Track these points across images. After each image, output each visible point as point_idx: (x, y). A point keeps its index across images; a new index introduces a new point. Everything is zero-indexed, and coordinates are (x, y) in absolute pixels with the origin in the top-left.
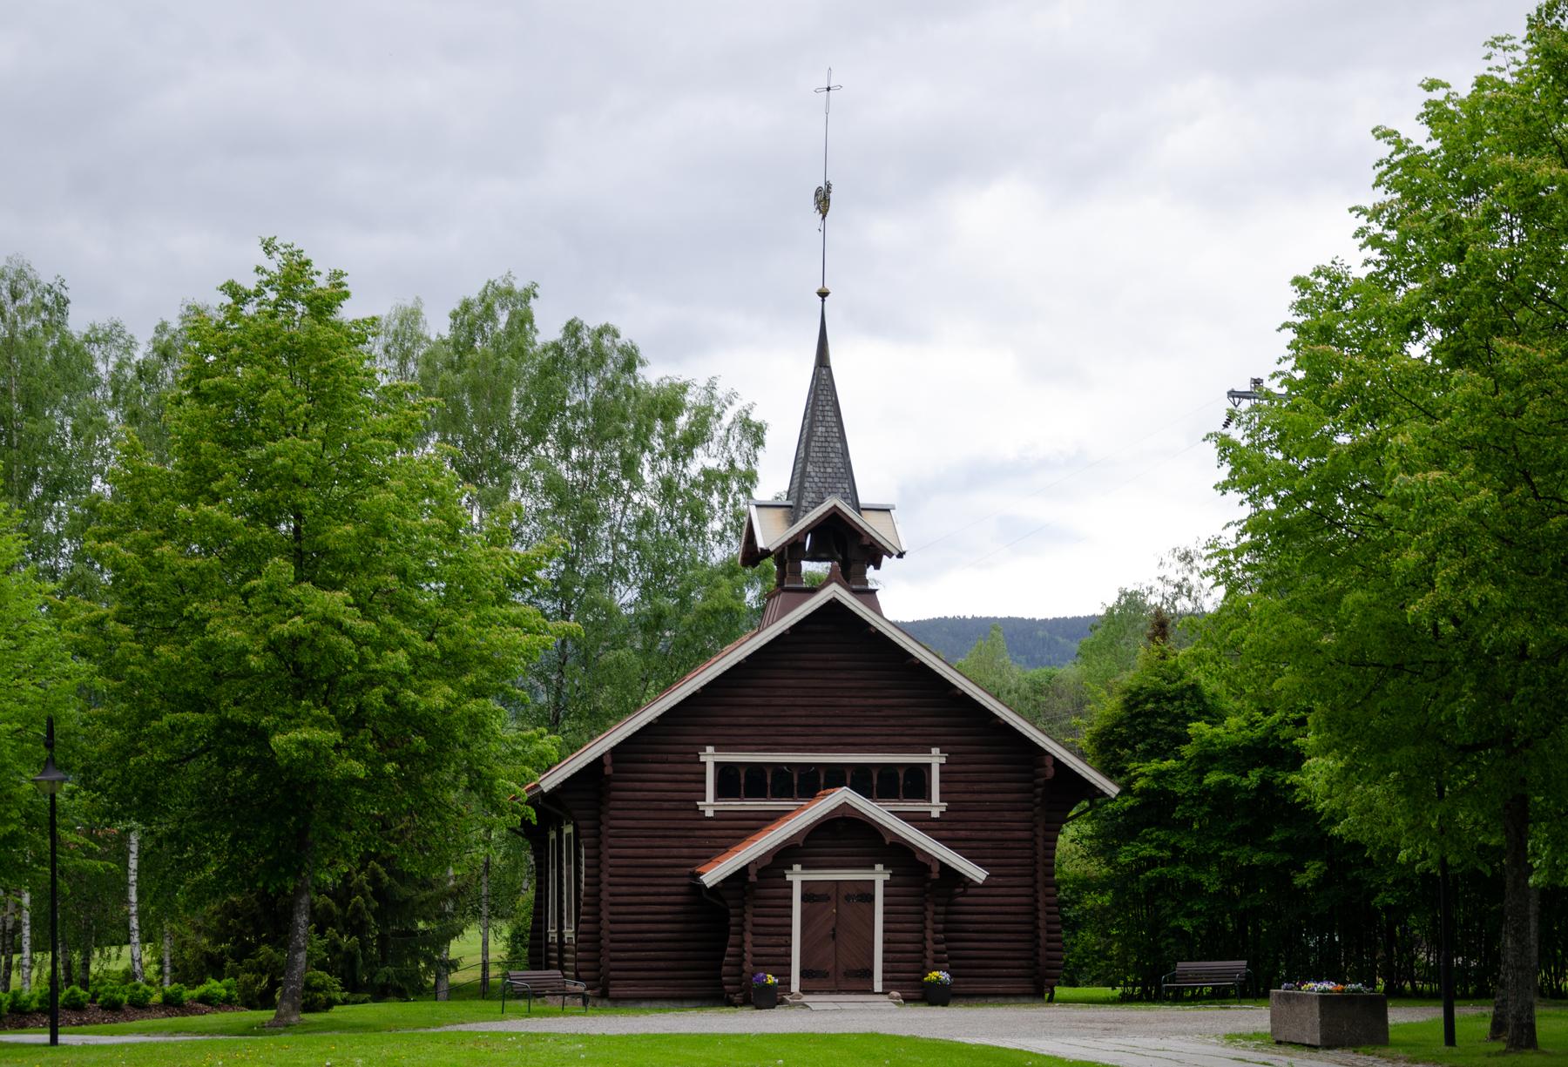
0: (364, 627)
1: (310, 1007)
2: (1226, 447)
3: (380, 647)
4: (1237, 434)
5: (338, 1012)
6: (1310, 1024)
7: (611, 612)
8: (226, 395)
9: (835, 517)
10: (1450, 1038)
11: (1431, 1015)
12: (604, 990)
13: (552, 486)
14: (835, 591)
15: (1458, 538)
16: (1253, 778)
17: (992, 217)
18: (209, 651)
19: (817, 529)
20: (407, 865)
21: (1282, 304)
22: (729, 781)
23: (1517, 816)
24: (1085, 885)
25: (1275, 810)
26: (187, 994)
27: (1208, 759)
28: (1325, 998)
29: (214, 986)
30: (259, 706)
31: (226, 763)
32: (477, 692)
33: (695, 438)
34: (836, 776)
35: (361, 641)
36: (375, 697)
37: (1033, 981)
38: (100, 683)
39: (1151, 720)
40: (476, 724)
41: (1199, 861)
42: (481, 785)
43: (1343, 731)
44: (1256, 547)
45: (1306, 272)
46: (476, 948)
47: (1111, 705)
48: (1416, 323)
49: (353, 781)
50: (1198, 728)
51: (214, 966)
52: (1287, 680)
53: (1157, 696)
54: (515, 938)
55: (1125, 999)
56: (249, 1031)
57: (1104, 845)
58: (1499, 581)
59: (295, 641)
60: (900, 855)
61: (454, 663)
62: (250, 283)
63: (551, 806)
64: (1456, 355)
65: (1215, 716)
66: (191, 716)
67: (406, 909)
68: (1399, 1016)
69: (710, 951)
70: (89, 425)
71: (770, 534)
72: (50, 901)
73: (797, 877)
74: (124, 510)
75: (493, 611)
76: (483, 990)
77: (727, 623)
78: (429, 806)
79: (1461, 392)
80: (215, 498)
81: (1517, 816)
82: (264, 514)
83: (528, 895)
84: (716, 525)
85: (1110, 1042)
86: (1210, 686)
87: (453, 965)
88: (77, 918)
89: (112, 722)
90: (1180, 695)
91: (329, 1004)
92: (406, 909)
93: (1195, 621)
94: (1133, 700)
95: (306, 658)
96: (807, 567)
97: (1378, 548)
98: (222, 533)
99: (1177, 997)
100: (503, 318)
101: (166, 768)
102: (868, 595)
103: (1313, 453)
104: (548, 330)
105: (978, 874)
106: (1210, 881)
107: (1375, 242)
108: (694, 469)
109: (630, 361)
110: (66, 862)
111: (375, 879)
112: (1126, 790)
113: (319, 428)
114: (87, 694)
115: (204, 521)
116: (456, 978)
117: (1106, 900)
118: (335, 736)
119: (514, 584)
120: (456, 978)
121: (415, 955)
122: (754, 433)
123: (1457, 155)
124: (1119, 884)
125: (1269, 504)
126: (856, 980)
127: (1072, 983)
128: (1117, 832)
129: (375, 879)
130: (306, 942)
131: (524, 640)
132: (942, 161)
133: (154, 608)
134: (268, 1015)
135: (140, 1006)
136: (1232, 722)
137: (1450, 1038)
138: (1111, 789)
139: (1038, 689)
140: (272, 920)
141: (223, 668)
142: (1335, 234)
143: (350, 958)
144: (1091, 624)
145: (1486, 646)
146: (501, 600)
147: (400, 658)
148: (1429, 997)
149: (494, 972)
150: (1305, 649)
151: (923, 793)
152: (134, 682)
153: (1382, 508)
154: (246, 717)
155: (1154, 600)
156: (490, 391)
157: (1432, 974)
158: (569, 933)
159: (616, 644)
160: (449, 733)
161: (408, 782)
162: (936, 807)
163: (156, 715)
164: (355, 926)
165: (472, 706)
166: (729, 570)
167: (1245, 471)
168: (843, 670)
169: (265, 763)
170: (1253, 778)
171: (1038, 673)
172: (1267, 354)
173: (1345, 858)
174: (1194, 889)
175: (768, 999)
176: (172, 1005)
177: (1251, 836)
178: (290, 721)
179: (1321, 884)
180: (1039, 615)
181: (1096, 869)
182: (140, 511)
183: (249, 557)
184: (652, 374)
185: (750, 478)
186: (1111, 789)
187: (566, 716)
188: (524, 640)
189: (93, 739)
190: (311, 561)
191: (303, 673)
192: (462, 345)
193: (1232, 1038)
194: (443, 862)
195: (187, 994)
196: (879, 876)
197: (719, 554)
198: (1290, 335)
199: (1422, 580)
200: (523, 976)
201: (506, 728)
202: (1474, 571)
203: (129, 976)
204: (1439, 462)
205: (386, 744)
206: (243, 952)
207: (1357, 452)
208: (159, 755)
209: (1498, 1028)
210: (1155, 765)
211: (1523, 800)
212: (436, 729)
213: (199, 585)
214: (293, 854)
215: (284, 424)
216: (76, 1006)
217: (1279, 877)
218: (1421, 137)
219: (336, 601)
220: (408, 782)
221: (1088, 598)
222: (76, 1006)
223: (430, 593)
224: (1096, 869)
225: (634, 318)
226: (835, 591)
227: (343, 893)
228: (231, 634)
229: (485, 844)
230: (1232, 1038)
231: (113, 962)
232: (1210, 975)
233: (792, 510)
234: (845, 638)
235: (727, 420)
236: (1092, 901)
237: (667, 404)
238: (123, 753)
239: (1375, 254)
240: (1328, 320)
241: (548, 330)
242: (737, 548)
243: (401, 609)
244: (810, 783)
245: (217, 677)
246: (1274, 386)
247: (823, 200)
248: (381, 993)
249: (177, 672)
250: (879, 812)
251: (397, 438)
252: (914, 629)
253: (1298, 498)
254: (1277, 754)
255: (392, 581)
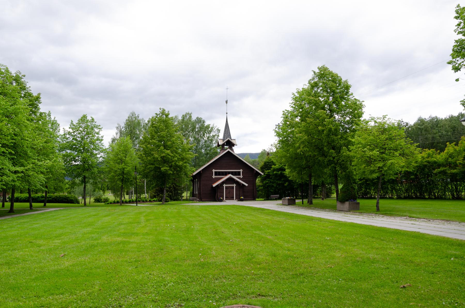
0: (172, 155)
1: (166, 202)
2: (275, 131)
3: (174, 157)
4: (277, 130)
5: (169, 202)
6: (286, 202)
7: (201, 153)
8: (155, 127)
9: (228, 141)
10: (303, 204)
11: (301, 201)
12: (201, 200)
13: (194, 137)
14: (229, 150)
15: (303, 142)
16: (279, 172)
17: (248, 102)
18: (154, 158)
19: (226, 142)
20: (177, 184)
21: (281, 114)
22: (216, 174)
23: (310, 176)
24: (259, 186)
25: (282, 176)
26: (152, 200)
27: (274, 170)
28: (288, 199)
29: (155, 199)
30: (159, 165)
31: (155, 171)
32: (185, 163)
33: (211, 131)
34: (229, 173)
35: (171, 156)
36: (173, 163)
37: (253, 198)
38: (141, 162)
39: (267, 166)
40: (185, 167)
41: (273, 183)
42: (186, 174)
43: (290, 166)
44: (279, 143)
45: (284, 110)
46: (186, 195)
47: (263, 163)
48: (297, 116)
49: (170, 174)
50: (273, 166)
51: (155, 197)
52: (283, 160)
53: (268, 162)
54: (190, 193)
55: (265, 200)
56: (159, 204)
57: (262, 180)
58: (308, 147)
59: (164, 157)
60: (237, 183)
61: (183, 159)
62: (158, 113)
63: (194, 177)
64: (302, 120)
65: (275, 165)
66: (152, 166)
67: (178, 190)
68: (297, 201)
69: (214, 195)
70: (140, 131)
71: (221, 143)
72: (136, 189)
73: (225, 185)
74: (144, 141)
75: (187, 153)
76: (187, 200)
77: (216, 154)
78: (180, 177)
79: (303, 125)
80: (154, 139)
81: (310, 176)
82: (160, 141)
83: (192, 188)
84: (214, 142)
85: (263, 205)
86: (274, 161)
87: (183, 197)
88: (139, 191)
89: (142, 167)
90: (271, 162)
91: (168, 201)
92: (178, 190)
93: (272, 153)
94: (265, 163)
95: (165, 159)
96: (225, 147)
97: (294, 144)
98: (155, 143)
99: (271, 200)
100: (188, 117)
101: (149, 172)
102: (232, 150)
103: (286, 133)
104: (194, 118)
105: (247, 185)
106: (275, 185)
107: (292, 107)
108: (211, 135)
109: (204, 122)
110: (138, 183)
111: (173, 186)
112: (264, 174)
113: (166, 130)
114: (140, 163)
115: (153, 142)
116: (183, 198)
117: (262, 188)
118: (168, 168)
119: (190, 149)
120: (183, 198)
121: (179, 196)
122: (219, 131)
123: (300, 97)
124: (263, 186)
125: (281, 138)
126: (232, 198)
127: (258, 198)
128: (263, 179)
129: (173, 186)
130: (166, 194)
131: (191, 156)
132: (243, 95)
133: (147, 153)
134: (161, 203)
135: (146, 201)
136: (277, 165)
137: (303, 204)
138: (263, 174)
139: (253, 162)
140: (161, 191)
141: (156, 160)
142: (287, 105)
143: (171, 196)
144: (259, 154)
145: (307, 156)
146: (188, 151)
147: (176, 159)
148: (300, 199)
149: (188, 198)
150: (285, 156)
151: (240, 175)
152: (145, 162)
153: (294, 139)
154: (158, 166)
155: (268, 150)
156: (187, 126)
157: (301, 196)
158: (197, 193)
159: (202, 157)
160: (182, 168)
161: (177, 174)
162: (241, 177)
163: (148, 166)
164: (172, 192)
165: (185, 164)
166: (216, 147)
167: (278, 135)
168: (231, 160)
169: (160, 172)
170: (279, 172)
171: (253, 160)
172: (279, 120)
173: (290, 182)
174: (273, 186)
175: (221, 201)
176: (150, 201)
177: (280, 180)
178: (163, 166)
179: (288, 185)
180: (254, 152)
181: (261, 184)
182: (146, 141)
183: (158, 146)
184: (206, 124)
185: (218, 136)
186: (263, 174)
187: (197, 165)
188: (191, 156)
189: (141, 169)
190: (166, 147)
191: (165, 160)
192: (183, 120)
193: (277, 204)
194: (182, 184)
195: (152, 200)
196: (235, 185)
197: (215, 145)
198: (283, 118)
199: (299, 148)
200: (191, 198)
201: (189, 167)
202: (305, 146)
203: (145, 198)
204: (301, 133)
205: (174, 169)
206: (158, 195)
207: (291, 132)
208: (148, 171)
209: (308, 202)
210: (268, 171)
211: (311, 174)
212: (181, 167)
213: (152, 150)
214: (164, 183)
215: (162, 130)
216: (139, 201)
217: (283, 184)
218: (297, 95)
219: (168, 152)
220: (177, 174)
221: (259, 151)
222: (139, 201)
223: (180, 151)
224: (261, 184)
225: (203, 116)
226: (229, 150)
227: (170, 188)
228: (156, 156)
229: (186, 182)
230: (277, 204)
231: (143, 196)
232: (275, 197)
233: (223, 140)
234: (230, 155)
235: (216, 129)
236: (260, 188)
237: (208, 127)
238: (144, 170)
239: (292, 108)
240: (287, 117)
241: (194, 118)
242: (217, 145)
243: (176, 153)
244: (226, 174)
245: (155, 161)
246: (280, 124)
247: (227, 102)
248: (174, 200)
249: (150, 160)
250: (234, 177)
251: (175, 131)
252: (238, 155)
253: (284, 138)
254: (283, 169)
255: (175, 149)
